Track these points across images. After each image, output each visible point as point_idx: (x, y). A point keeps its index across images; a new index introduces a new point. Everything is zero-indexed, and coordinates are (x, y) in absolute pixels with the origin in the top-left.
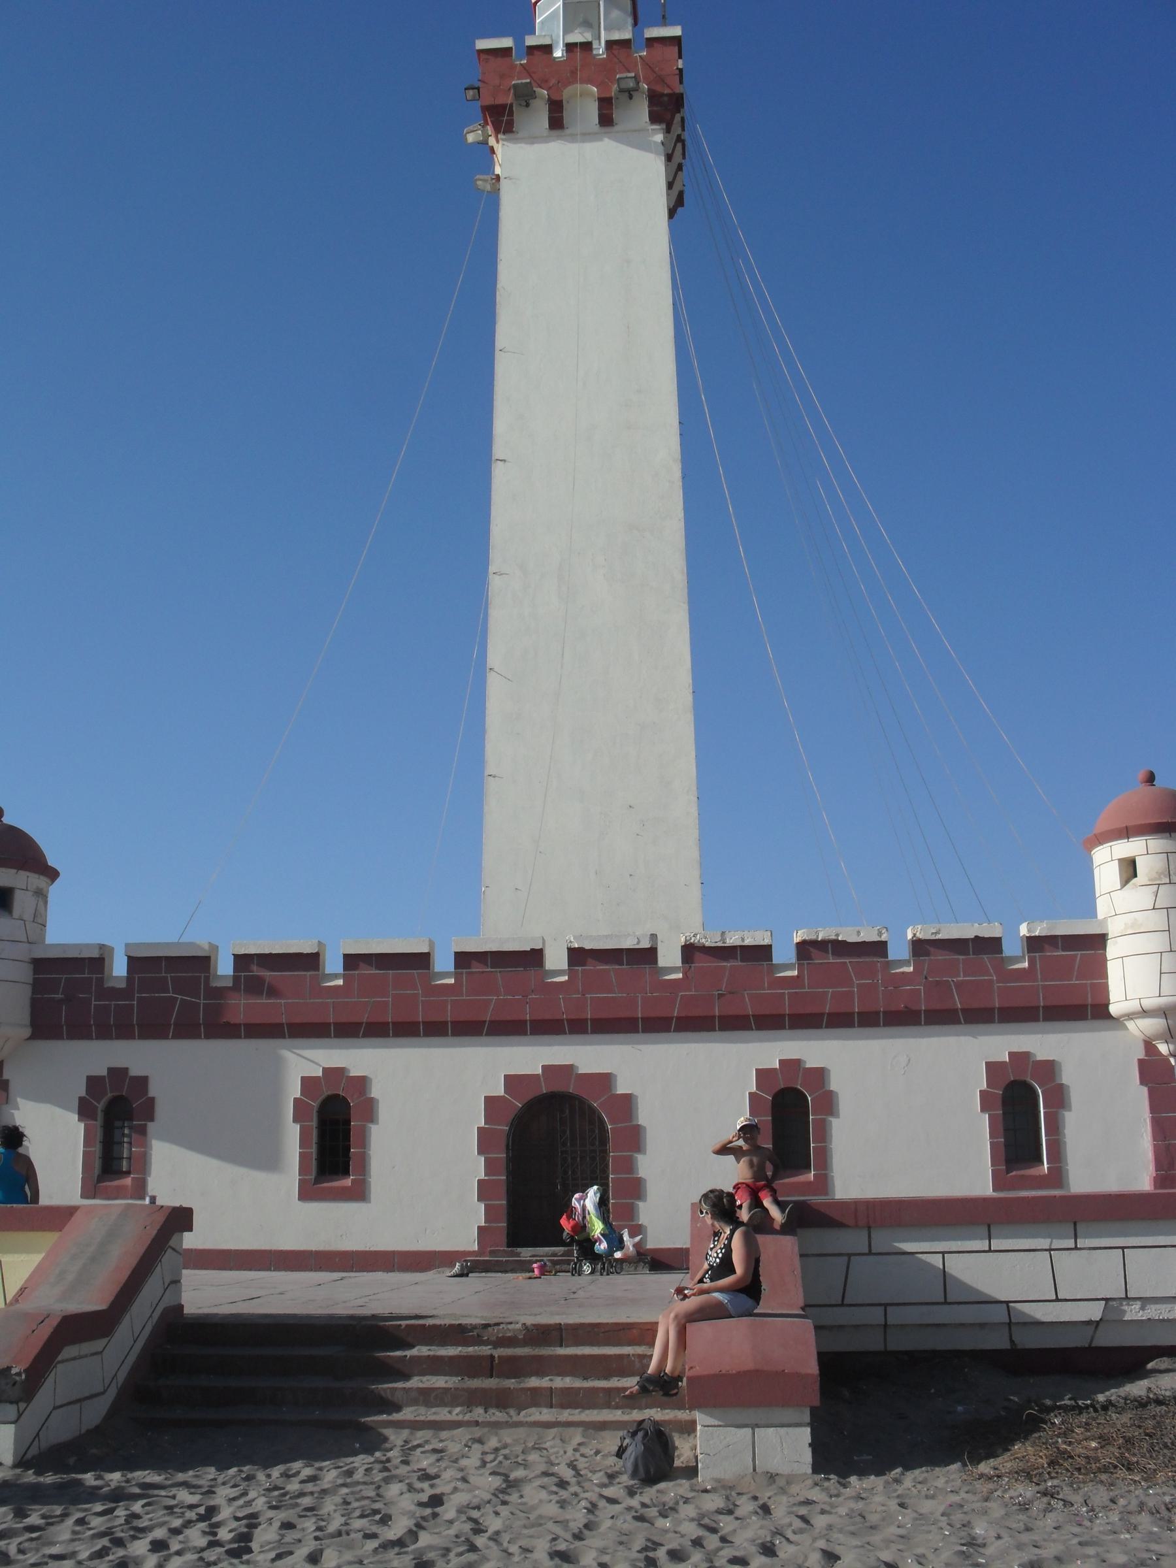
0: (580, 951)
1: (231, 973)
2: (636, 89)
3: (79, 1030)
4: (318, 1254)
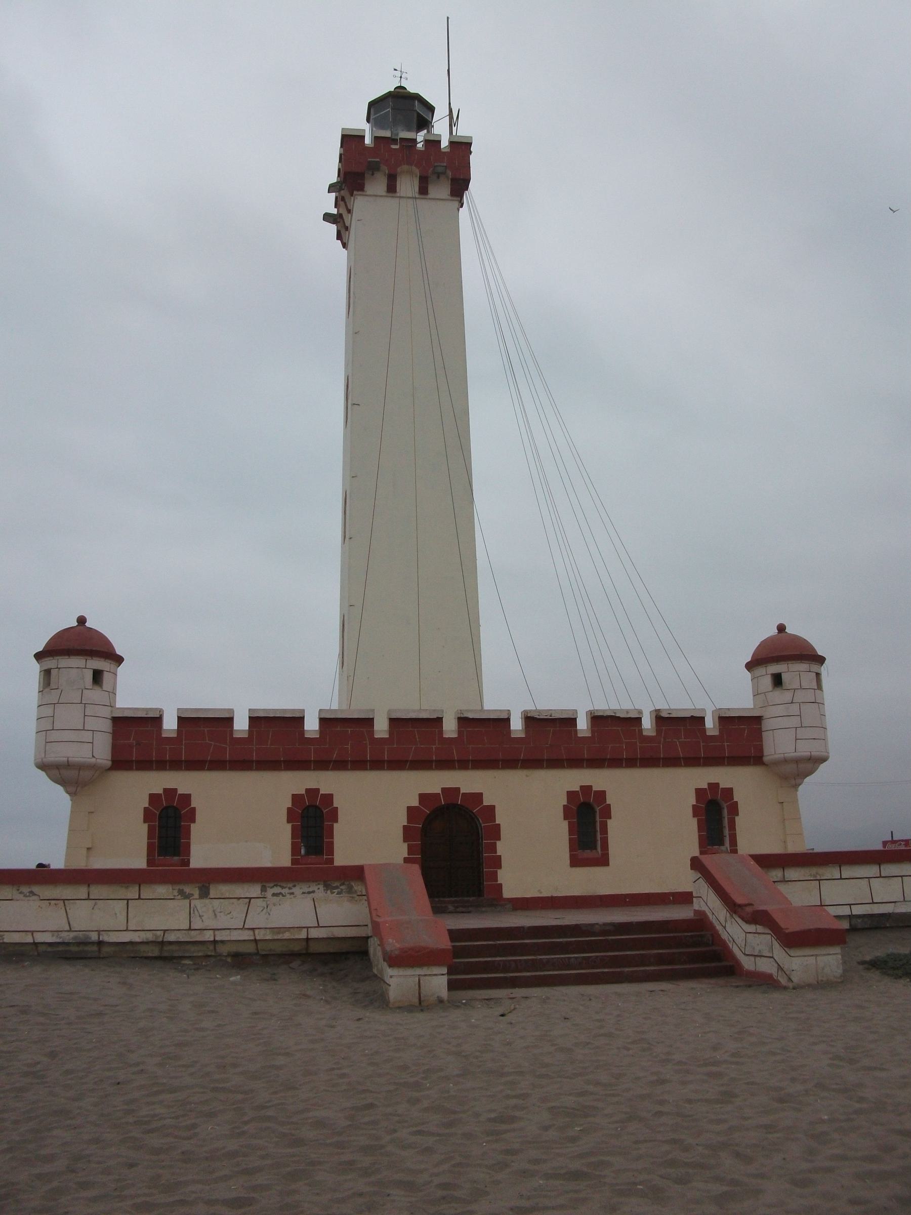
0: (466, 719)
1: (176, 728)
2: (444, 173)
3: (145, 765)
4: (674, 894)
